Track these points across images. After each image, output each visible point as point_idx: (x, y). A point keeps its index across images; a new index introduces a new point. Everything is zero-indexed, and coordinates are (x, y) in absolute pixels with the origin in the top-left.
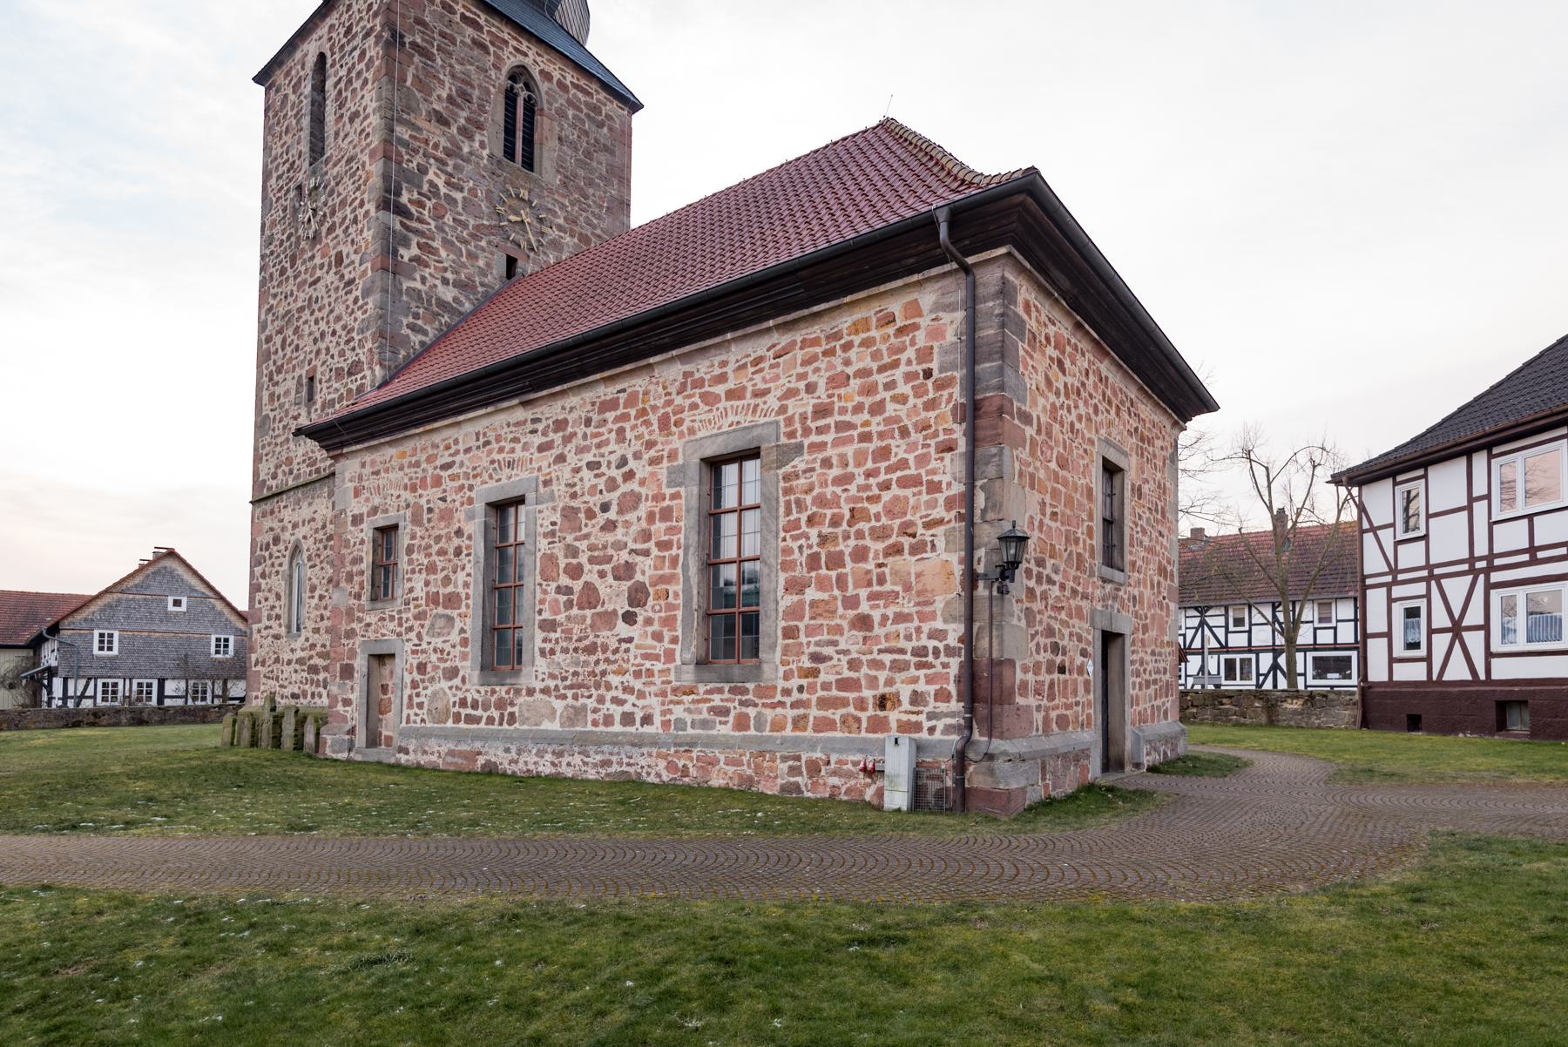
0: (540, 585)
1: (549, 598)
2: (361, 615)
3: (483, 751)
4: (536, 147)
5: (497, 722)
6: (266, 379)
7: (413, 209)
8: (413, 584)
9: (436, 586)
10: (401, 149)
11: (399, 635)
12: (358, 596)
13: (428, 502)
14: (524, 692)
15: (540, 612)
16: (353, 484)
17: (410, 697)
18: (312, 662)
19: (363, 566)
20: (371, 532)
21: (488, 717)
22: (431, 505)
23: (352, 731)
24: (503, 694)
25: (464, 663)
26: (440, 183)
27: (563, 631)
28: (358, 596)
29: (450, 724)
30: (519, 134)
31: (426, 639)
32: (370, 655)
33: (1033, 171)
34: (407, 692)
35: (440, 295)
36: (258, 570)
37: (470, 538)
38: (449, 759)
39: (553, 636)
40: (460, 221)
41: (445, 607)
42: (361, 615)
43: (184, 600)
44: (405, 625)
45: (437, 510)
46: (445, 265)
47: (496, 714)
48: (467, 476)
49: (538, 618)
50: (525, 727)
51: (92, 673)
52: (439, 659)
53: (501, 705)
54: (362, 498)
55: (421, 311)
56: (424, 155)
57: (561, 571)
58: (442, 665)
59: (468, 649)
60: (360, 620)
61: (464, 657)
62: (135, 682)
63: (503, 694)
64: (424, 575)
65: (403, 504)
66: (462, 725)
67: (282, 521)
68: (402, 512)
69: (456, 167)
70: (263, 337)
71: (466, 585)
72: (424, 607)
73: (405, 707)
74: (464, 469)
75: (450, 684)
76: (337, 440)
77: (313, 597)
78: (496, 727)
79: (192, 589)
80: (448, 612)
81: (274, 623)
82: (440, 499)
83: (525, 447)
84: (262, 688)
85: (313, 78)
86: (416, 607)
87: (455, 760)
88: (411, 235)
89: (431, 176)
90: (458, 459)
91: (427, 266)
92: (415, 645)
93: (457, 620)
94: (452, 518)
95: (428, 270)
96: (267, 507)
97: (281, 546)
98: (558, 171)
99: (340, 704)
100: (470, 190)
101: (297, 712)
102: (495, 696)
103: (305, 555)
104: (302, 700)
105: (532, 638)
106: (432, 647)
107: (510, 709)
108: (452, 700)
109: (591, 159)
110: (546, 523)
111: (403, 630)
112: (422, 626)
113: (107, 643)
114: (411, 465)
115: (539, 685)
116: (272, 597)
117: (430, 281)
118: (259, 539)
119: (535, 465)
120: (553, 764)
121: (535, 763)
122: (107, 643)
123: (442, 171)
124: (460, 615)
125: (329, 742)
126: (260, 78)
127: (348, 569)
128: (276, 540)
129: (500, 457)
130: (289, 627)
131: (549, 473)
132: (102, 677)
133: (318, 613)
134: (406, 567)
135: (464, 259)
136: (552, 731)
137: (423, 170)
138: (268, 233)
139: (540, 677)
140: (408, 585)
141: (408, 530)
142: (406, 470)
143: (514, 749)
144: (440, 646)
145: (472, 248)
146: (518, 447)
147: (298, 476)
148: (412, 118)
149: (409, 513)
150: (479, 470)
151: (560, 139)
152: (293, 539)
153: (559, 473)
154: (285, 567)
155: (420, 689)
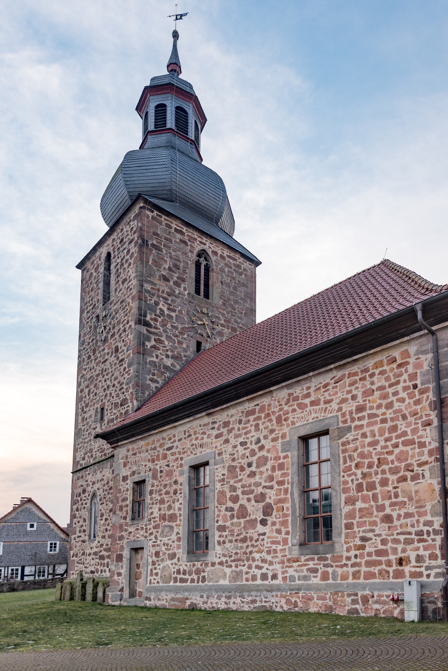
0: (217, 507)
1: (222, 514)
2: (126, 528)
3: (189, 597)
5: (196, 582)
6: (80, 410)
7: (152, 323)
8: (153, 510)
11: (146, 537)
12: (125, 518)
13: (160, 467)
14: (210, 565)
15: (217, 521)
16: (123, 460)
18: (101, 554)
19: (128, 502)
22: (162, 469)
24: (199, 566)
25: (179, 551)
26: (165, 309)
28: (125, 518)
29: (172, 583)
31: (159, 538)
34: (150, 567)
35: (165, 363)
36: (75, 507)
37: (181, 484)
38: (172, 603)
39: (224, 534)
40: (174, 326)
42: (126, 528)
43: (35, 524)
44: (149, 532)
45: (165, 471)
46: (167, 348)
47: (195, 577)
49: (216, 525)
50: (211, 583)
52: (166, 549)
53: (198, 572)
54: (127, 468)
55: (156, 372)
56: (158, 296)
57: (228, 499)
58: (168, 552)
59: (181, 543)
60: (126, 530)
61: (179, 547)
63: (199, 566)
64: (158, 505)
65: (148, 469)
66: (178, 584)
67: (87, 481)
68: (147, 473)
69: (172, 301)
70: (79, 390)
71: (180, 509)
72: (158, 522)
73: (149, 575)
74: (178, 450)
75: (172, 562)
76: (116, 439)
77: (102, 520)
80: (171, 524)
81: (82, 534)
83: (209, 437)
84: (76, 569)
85: (105, 264)
86: (154, 522)
88: (151, 335)
89: (161, 306)
90: (175, 444)
93: (175, 528)
94: (172, 475)
95: (159, 351)
96: (79, 474)
97: (87, 494)
98: (221, 298)
99: (116, 575)
101: (93, 581)
102: (195, 567)
104: (96, 574)
105: (214, 536)
106: (162, 542)
108: (173, 570)
110: (220, 475)
111: (148, 534)
112: (157, 532)
114: (152, 449)
115: (217, 561)
116: (81, 521)
117: (160, 357)
118: (75, 491)
119: (214, 445)
120: (226, 603)
121: (216, 603)
124: (176, 525)
125: (110, 596)
127: (120, 504)
128: (84, 491)
130: (90, 536)
131: (221, 449)
133: (105, 528)
134: (149, 501)
135: (176, 345)
137: (157, 304)
138: (82, 339)
139: (218, 556)
140: (150, 511)
141: (150, 482)
142: (149, 452)
144: (166, 542)
145: (180, 339)
146: (205, 436)
147: (95, 458)
149: (151, 474)
150: (185, 450)
151: (222, 282)
152: (92, 490)
154: (88, 505)
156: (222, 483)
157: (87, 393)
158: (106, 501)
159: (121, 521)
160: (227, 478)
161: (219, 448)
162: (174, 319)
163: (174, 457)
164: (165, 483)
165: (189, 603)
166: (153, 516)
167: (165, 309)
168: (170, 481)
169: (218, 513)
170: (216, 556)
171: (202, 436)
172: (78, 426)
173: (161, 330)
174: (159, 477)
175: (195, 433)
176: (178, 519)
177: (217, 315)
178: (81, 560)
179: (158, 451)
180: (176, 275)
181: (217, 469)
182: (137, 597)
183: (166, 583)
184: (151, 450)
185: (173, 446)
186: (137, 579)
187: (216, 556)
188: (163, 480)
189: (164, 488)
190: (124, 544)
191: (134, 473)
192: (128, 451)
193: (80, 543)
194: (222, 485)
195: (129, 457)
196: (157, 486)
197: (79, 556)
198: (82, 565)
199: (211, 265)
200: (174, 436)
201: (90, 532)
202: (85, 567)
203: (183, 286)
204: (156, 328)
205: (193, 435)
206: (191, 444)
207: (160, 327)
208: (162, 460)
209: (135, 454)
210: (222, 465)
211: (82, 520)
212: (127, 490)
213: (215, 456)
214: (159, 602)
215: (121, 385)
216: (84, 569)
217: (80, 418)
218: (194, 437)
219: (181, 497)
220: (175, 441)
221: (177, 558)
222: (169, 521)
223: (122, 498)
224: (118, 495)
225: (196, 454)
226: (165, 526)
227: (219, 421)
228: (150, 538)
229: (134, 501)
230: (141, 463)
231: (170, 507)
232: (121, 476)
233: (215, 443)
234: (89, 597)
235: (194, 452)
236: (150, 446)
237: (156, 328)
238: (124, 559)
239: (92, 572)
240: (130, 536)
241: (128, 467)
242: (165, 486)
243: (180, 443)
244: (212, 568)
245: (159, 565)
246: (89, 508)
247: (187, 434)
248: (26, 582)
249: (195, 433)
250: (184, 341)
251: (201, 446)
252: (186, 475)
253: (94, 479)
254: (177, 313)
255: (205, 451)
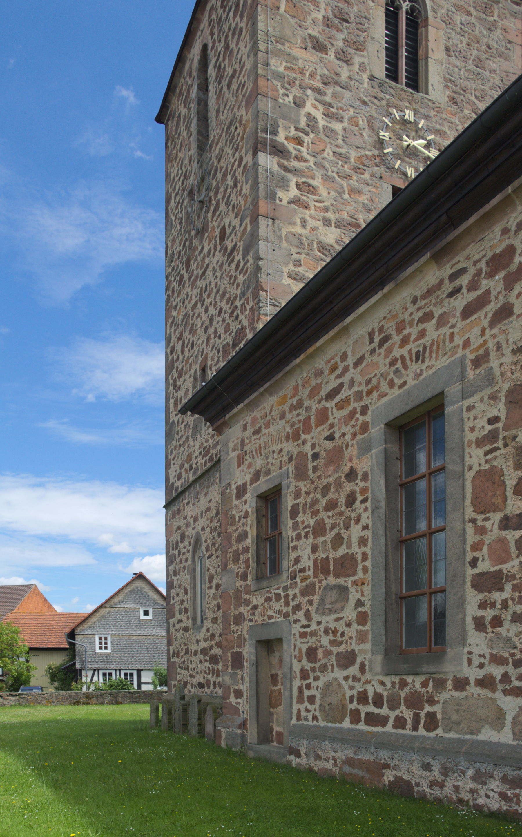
0: (473, 521)
1: (488, 539)
2: (247, 597)
4: (421, 64)
5: (409, 726)
6: (171, 388)
7: (290, 146)
8: (299, 552)
9: (325, 551)
10: (276, 83)
11: (286, 615)
12: (244, 577)
13: (313, 446)
14: (450, 684)
15: (474, 563)
16: (237, 453)
17: (300, 689)
18: (212, 652)
19: (249, 541)
20: (254, 500)
21: (397, 718)
22: (317, 450)
23: (243, 725)
24: (418, 686)
25: (362, 646)
26: (318, 115)
27: (515, 588)
28: (244, 577)
29: (346, 724)
30: (403, 53)
31: (316, 617)
32: (258, 642)
33: (476, 567)
34: (297, 683)
35: (322, 238)
36: (171, 568)
37: (365, 478)
38: (347, 769)
39: (497, 596)
40: (340, 154)
41: (337, 576)
42: (247, 597)
43: (151, 611)
44: (292, 604)
45: (323, 454)
46: (326, 204)
47: (408, 715)
48: (359, 396)
49: (470, 572)
50: (452, 735)
51: (96, 666)
52: (332, 643)
54: (244, 467)
55: (302, 257)
56: (301, 87)
57: (509, 493)
58: (335, 650)
59: (368, 627)
60: (247, 602)
61: (362, 637)
62: (122, 673)
63: (418, 686)
64: (311, 540)
65: (285, 458)
66: (362, 726)
67: (185, 518)
68: (284, 468)
69: (335, 95)
70: (169, 351)
71: (363, 541)
72: (312, 579)
73: (294, 701)
74: (356, 388)
75: (345, 673)
77: (210, 587)
78: (408, 731)
79: (156, 603)
80: (341, 581)
81: (183, 617)
82: (326, 438)
83: (442, 321)
84: (178, 677)
85: (199, 78)
86: (304, 579)
87: (355, 771)
88: (289, 176)
89: (308, 108)
90: (346, 379)
91: (307, 207)
92: (304, 627)
93: (352, 590)
94: (341, 457)
95: (307, 212)
96: (175, 508)
97: (186, 543)
98: (446, 86)
99: (232, 695)
100: (351, 119)
101: (199, 701)
102: (407, 690)
103: (204, 545)
104: (206, 689)
105: (461, 604)
106: (322, 627)
107: (428, 708)
108: (349, 693)
109: (483, 68)
110: (482, 422)
111: (290, 609)
112: (311, 603)
113: (103, 645)
114: (293, 408)
116: (181, 592)
117: (311, 223)
118: (171, 540)
119: (459, 341)
120: (503, 796)
121: (472, 791)
122: (103, 645)
123: (320, 102)
124: (355, 583)
125: (224, 735)
126: (159, 119)
127: (235, 548)
128: (183, 537)
129: (404, 351)
130: (194, 619)
131: (485, 342)
132: (102, 669)
133: (215, 602)
134: (290, 533)
135: (346, 196)
136: (498, 745)
137: (299, 104)
138: (170, 252)
139: (476, 661)
140: (294, 555)
141: (292, 489)
142: (288, 416)
143: (436, 767)
144: (332, 625)
145: (353, 182)
146: (430, 326)
147: (196, 469)
148: (287, 47)
149: (291, 468)
150: (374, 382)
151: (447, 49)
152: (194, 532)
153: (501, 338)
154: (190, 562)
155: (311, 680)
156: (488, 447)
157: (179, 352)
158: (217, 550)
159: (238, 584)
160: (506, 428)
161: (476, 342)
162: (340, 137)
163: (345, 412)
164: (324, 481)
165: (392, 779)
166: (300, 566)
167: (318, 115)
168: (336, 476)
169: (477, 538)
170: (470, 662)
171: (421, 326)
172: (169, 419)
173: (311, 164)
174: (310, 472)
175: (400, 328)
176: (360, 567)
177: (438, 127)
178: (184, 662)
179: (307, 409)
180: (341, 36)
181: (470, 408)
182: (275, 744)
183: (334, 721)
184: (291, 411)
185: (342, 385)
186: (273, 705)
187: (470, 662)
188: (319, 477)
189: (323, 496)
190: (245, 632)
191: (256, 476)
192: (245, 428)
193: (182, 632)
194: (486, 454)
195: (247, 441)
196: (308, 493)
197: (181, 655)
198: (186, 672)
199: (422, 10)
200: (344, 357)
201: (195, 613)
202: (192, 676)
203: (357, 60)
204: (299, 158)
205: (394, 333)
206: (388, 361)
207: (308, 157)
208: (317, 426)
209: (257, 432)
210: (488, 391)
211: (182, 591)
212: (246, 515)
213: (463, 371)
214: (318, 763)
215: (232, 303)
216: (189, 678)
217: (172, 401)
218: (396, 339)
219: (366, 509)
220: (346, 369)
221: (357, 665)
222: (337, 576)
223: (236, 534)
224: (231, 529)
225: (405, 383)
226: (329, 588)
227: (475, 263)
228: (295, 617)
229: (259, 538)
230: (271, 449)
231: (338, 541)
232: (234, 487)
233: (463, 330)
234: (194, 731)
235: (398, 382)
236: (288, 404)
237: (299, 158)
238: (245, 664)
239: (201, 685)
240: (254, 614)
241: (246, 463)
242: (326, 489)
243: (359, 369)
244: (455, 694)
245: (316, 679)
246: (191, 567)
247: (377, 339)
248: (144, 692)
249: (400, 328)
250: (366, 189)
251: (419, 357)
252: (377, 450)
253: (197, 512)
254: (346, 124)
255: (429, 367)
